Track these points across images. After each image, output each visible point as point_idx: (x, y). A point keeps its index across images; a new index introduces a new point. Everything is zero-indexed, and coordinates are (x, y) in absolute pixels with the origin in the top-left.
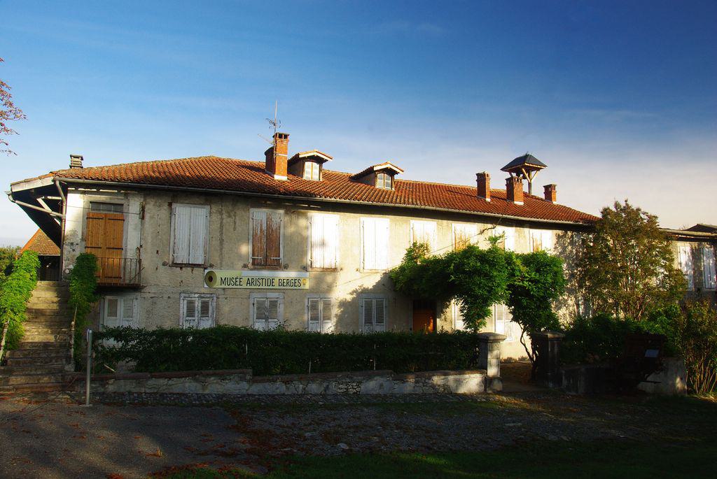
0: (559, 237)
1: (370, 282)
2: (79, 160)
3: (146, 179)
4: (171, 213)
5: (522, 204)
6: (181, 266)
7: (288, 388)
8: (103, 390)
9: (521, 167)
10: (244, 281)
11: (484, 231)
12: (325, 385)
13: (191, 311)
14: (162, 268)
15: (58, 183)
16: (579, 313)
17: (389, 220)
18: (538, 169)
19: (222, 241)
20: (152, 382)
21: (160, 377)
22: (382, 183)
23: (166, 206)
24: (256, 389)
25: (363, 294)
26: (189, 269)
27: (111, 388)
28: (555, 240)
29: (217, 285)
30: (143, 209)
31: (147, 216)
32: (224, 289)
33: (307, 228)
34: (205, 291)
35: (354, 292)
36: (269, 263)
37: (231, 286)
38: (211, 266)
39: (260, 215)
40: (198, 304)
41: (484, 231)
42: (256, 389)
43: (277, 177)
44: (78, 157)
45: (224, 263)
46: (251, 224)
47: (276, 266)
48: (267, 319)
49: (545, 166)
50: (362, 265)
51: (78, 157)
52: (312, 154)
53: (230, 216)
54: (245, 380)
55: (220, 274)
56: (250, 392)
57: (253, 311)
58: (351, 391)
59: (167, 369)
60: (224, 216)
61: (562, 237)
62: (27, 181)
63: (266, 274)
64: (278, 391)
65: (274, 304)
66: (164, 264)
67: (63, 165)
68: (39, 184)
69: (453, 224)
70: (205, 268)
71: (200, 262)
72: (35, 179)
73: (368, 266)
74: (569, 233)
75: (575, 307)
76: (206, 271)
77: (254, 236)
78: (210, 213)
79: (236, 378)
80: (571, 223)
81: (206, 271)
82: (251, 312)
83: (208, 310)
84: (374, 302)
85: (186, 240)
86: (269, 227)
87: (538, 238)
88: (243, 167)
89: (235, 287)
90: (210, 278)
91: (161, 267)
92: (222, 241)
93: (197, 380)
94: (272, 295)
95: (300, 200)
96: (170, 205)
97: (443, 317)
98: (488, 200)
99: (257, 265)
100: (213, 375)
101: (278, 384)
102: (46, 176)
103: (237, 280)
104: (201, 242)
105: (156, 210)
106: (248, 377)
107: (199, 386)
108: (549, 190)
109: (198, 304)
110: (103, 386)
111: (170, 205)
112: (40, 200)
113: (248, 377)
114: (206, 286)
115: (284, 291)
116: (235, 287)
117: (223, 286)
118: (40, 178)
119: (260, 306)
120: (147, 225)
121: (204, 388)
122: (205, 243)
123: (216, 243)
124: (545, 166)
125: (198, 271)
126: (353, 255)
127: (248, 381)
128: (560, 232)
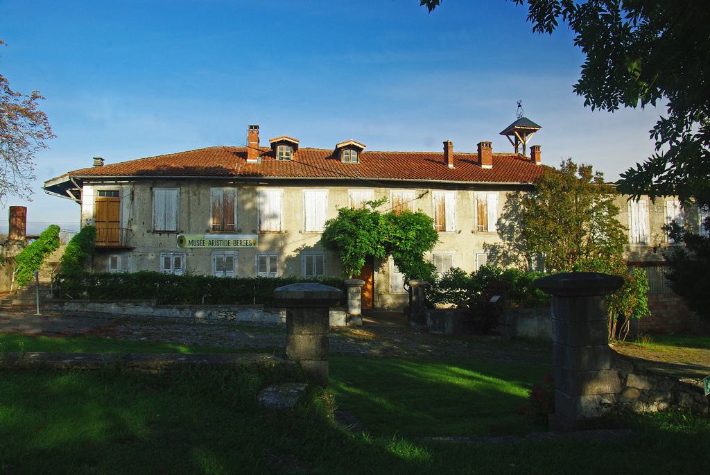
0: (509, 197)
1: (312, 242)
2: (100, 160)
3: (141, 173)
4: (152, 195)
5: (490, 167)
6: (160, 232)
7: (181, 313)
8: (61, 309)
9: (520, 129)
10: (207, 241)
11: (423, 195)
12: (209, 312)
13: (167, 265)
14: (147, 235)
15: (72, 179)
16: (531, 268)
17: (328, 190)
18: (535, 131)
19: (189, 213)
20: (91, 305)
21: (95, 302)
22: (351, 158)
23: (148, 190)
24: (158, 312)
25: (305, 251)
26: (166, 234)
27: (66, 307)
28: (506, 200)
29: (187, 245)
30: (133, 193)
31: (136, 198)
32: (192, 248)
33: (262, 204)
34: (178, 250)
35: (297, 250)
36: (225, 228)
37: (196, 247)
38: (182, 232)
39: (217, 192)
40: (173, 260)
41: (423, 195)
42: (158, 312)
43: (484, 167)
44: (98, 159)
45: (191, 230)
46: (211, 200)
47: (232, 230)
48: (225, 270)
49: (540, 127)
50: (303, 227)
51: (98, 159)
52: (349, 144)
53: (195, 195)
54: (151, 306)
55: (188, 238)
56: (154, 314)
57: (214, 265)
58: (229, 318)
59: (102, 298)
60: (191, 195)
61: (513, 197)
62: (54, 180)
63: (227, 237)
64: (174, 315)
65: (230, 259)
66: (148, 232)
67: (89, 164)
68: (61, 181)
69: (349, 190)
70: (178, 234)
71: (174, 229)
72: (59, 178)
73: (309, 229)
74: (522, 193)
75: (527, 262)
76: (178, 236)
77: (214, 208)
78: (180, 193)
79: (145, 305)
80: (519, 183)
81: (178, 236)
82: (213, 264)
83: (165, 262)
84: (314, 258)
85: (163, 214)
86: (225, 201)
87: (483, 199)
88: (461, 160)
89: (199, 247)
90: (181, 241)
91: (146, 233)
92: (189, 213)
93: (118, 305)
94: (230, 253)
95: (253, 181)
96: (151, 189)
97: (381, 270)
98: (451, 166)
99: (223, 230)
100: (130, 302)
101: (174, 310)
102: (65, 175)
103: (201, 242)
104: (174, 215)
105: (141, 192)
106: (153, 304)
107: (120, 309)
108: (534, 149)
109: (173, 260)
110: (61, 306)
111: (151, 189)
112: (68, 192)
113: (153, 304)
114: (178, 246)
115: (238, 250)
116: (199, 247)
117: (191, 247)
118: (62, 177)
119: (219, 261)
120: (135, 204)
121: (124, 310)
122: (177, 215)
123: (185, 215)
124: (540, 127)
125: (172, 236)
126: (298, 217)
127: (153, 307)
128: (511, 192)
